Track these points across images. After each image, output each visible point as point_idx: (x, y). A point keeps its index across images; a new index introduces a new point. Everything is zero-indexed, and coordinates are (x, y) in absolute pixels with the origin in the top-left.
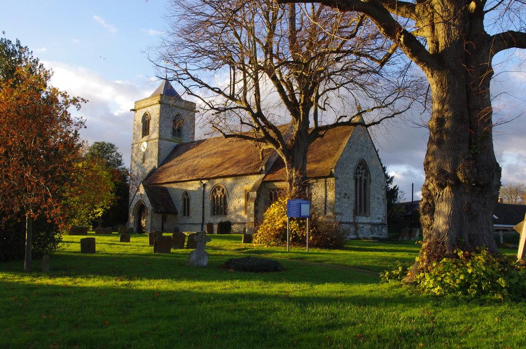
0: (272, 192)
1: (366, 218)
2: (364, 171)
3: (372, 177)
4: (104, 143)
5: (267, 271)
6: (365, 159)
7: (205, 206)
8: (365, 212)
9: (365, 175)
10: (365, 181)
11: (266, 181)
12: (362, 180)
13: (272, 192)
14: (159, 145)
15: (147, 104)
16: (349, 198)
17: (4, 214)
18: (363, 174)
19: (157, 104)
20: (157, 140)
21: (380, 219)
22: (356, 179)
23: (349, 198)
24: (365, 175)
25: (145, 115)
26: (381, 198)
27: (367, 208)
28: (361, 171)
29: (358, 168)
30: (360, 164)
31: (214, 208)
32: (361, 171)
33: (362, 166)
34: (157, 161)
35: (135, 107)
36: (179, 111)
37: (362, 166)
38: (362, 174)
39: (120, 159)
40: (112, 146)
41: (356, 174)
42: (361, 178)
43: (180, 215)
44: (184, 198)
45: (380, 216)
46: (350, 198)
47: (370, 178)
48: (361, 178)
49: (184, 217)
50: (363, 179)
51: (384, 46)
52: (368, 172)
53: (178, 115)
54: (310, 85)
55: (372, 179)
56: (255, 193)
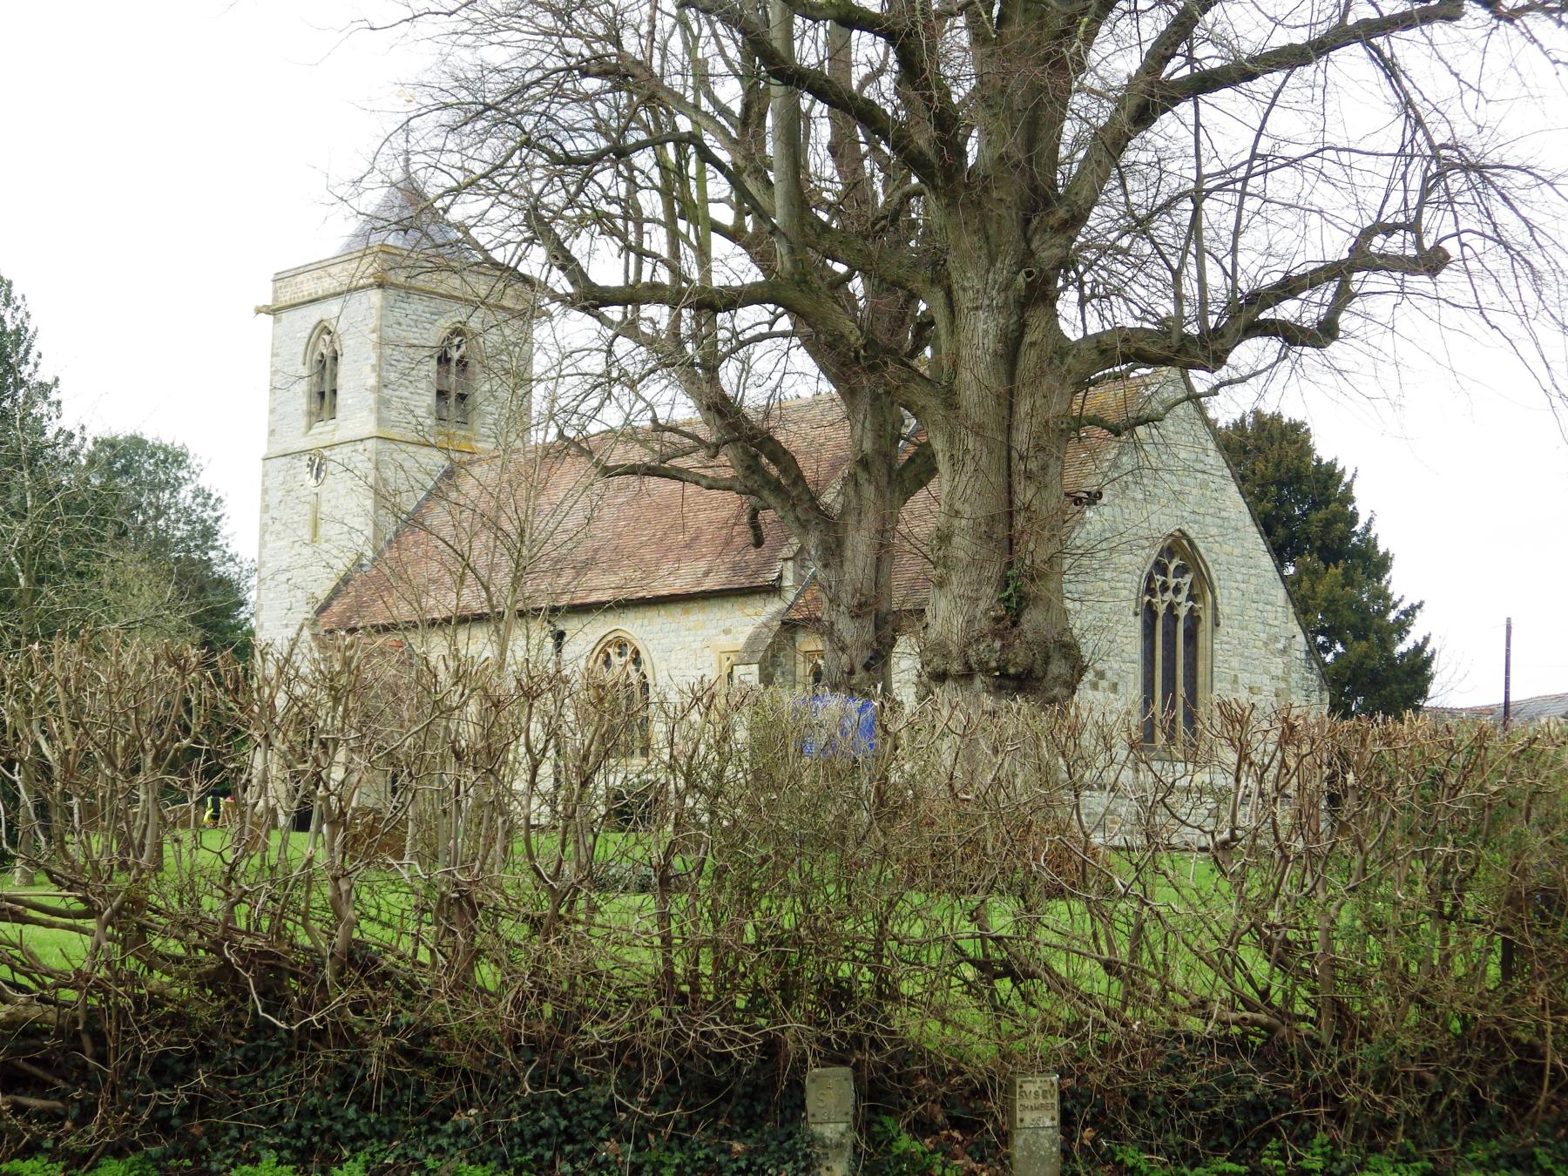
2: (1188, 578)
4: (137, 443)
10: (1193, 620)
11: (760, 302)
12: (1176, 618)
15: (328, 285)
16: (1114, 688)
17: (1562, 10)
22: (1150, 613)
23: (1114, 688)
24: (1191, 597)
25: (323, 329)
28: (1172, 582)
29: (1160, 567)
30: (1169, 552)
32: (1172, 582)
33: (1176, 562)
35: (275, 299)
36: (315, 313)
37: (1176, 562)
39: (208, 514)
40: (177, 458)
41: (1150, 591)
42: (1171, 607)
46: (1120, 687)
48: (1171, 607)
50: (1182, 612)
52: (1202, 585)
53: (457, 332)
55: (1224, 609)
56: (755, 668)
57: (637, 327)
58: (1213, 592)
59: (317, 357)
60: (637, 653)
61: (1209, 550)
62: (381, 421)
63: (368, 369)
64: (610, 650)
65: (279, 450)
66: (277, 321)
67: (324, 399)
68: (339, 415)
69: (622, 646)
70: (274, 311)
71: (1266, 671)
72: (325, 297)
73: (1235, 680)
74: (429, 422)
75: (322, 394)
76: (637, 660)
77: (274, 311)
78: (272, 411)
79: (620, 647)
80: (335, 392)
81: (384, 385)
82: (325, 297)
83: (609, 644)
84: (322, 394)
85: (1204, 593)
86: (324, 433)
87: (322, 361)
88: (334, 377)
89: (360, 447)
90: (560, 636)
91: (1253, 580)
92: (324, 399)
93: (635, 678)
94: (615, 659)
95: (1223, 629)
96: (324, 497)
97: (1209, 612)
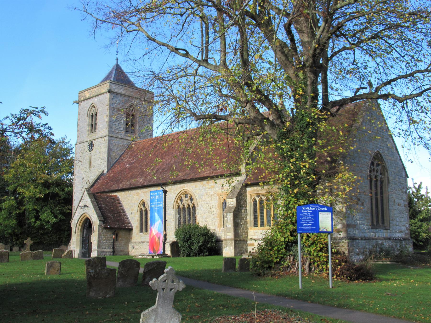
0: (256, 198)
1: (385, 231)
2: (380, 167)
3: (389, 176)
5: (205, 179)
6: (381, 151)
7: (167, 218)
8: (383, 223)
9: (381, 174)
10: (382, 182)
13: (256, 198)
14: (109, 144)
15: (94, 94)
16: (363, 204)
18: (379, 172)
19: (106, 92)
20: (106, 138)
21: (402, 232)
24: (381, 174)
26: (403, 204)
27: (385, 219)
28: (376, 169)
29: (372, 163)
31: (179, 208)
34: (106, 164)
36: (90, 102)
38: (377, 172)
43: (136, 231)
44: (141, 209)
45: (403, 228)
46: (365, 204)
47: (388, 178)
49: (141, 233)
50: (379, 178)
51: (201, 15)
54: (318, 65)
55: (391, 178)
56: (234, 200)
57: (208, 62)
58: (387, 172)
59: (91, 114)
60: (191, 197)
61: (386, 158)
62: (109, 133)
63: (105, 116)
64: (182, 196)
65: (79, 141)
66: (80, 105)
67: (93, 127)
68: (97, 130)
69: (186, 195)
70: (78, 102)
71: (402, 199)
72: (93, 97)
73: (394, 202)
74: (121, 248)
75: (92, 125)
76: (191, 199)
77: (78, 102)
78: (78, 131)
79: (185, 195)
80: (96, 124)
81: (110, 121)
82: (93, 97)
83: (182, 194)
84: (92, 125)
85: (384, 172)
86: (93, 136)
87: (92, 116)
88: (96, 120)
89: (103, 139)
90: (165, 192)
91: (397, 169)
92: (93, 127)
93: (191, 205)
94: (184, 199)
95: (390, 185)
96: (93, 154)
97: (386, 178)
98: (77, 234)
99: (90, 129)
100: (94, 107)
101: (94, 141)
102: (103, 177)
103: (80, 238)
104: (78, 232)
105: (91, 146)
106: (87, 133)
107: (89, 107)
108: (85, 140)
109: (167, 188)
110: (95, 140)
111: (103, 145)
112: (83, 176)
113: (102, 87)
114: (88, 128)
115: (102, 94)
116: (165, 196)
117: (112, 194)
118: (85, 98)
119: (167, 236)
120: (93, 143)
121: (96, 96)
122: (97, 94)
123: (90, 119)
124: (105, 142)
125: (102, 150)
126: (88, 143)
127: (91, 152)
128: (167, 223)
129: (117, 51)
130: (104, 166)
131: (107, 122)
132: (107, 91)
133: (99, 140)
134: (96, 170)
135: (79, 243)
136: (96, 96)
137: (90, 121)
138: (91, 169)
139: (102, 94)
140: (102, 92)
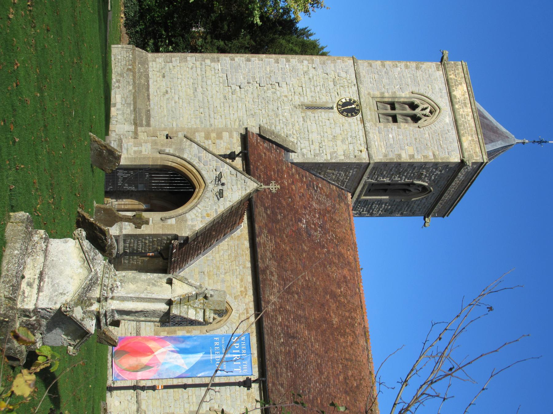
36: (443, 102)
59: (417, 102)
89: (363, 148)
90: (247, 384)
98: (157, 159)
99: (386, 100)
100: (431, 112)
101: (359, 116)
102: (283, 153)
103: (149, 165)
104: (161, 158)
105: (349, 109)
106: (377, 94)
107: (433, 98)
108: (362, 90)
109: (255, 386)
110: (363, 121)
111: (351, 147)
112: (284, 85)
113: (475, 137)
114: (388, 96)
115: (460, 140)
116: (239, 384)
117: (245, 217)
118: (452, 83)
119: (151, 391)
120: (356, 114)
121: (456, 121)
122: (460, 122)
123: (406, 100)
124: (357, 153)
125: (339, 143)
126: (356, 98)
127: (335, 109)
128: (180, 390)
129: (541, 142)
130: (304, 151)
131: (399, 156)
132: (465, 160)
133: (362, 133)
134: (297, 127)
135: (137, 163)
136: (456, 121)
137: (402, 100)
138: (298, 111)
139: (460, 140)
140: (463, 139)
